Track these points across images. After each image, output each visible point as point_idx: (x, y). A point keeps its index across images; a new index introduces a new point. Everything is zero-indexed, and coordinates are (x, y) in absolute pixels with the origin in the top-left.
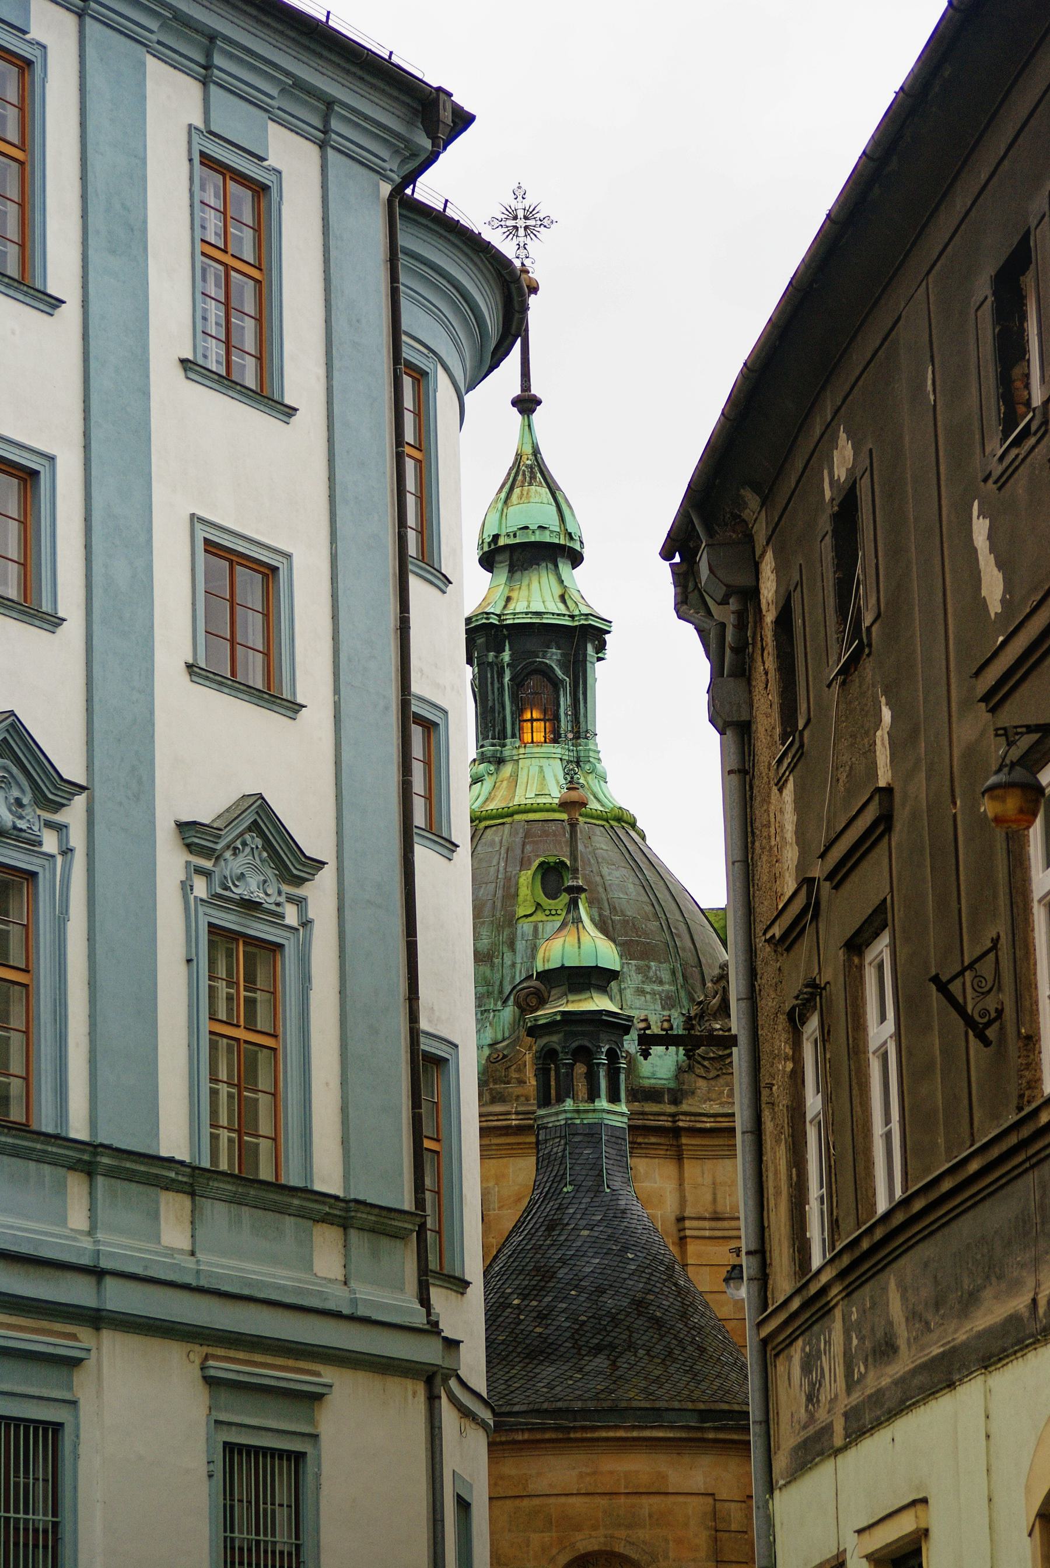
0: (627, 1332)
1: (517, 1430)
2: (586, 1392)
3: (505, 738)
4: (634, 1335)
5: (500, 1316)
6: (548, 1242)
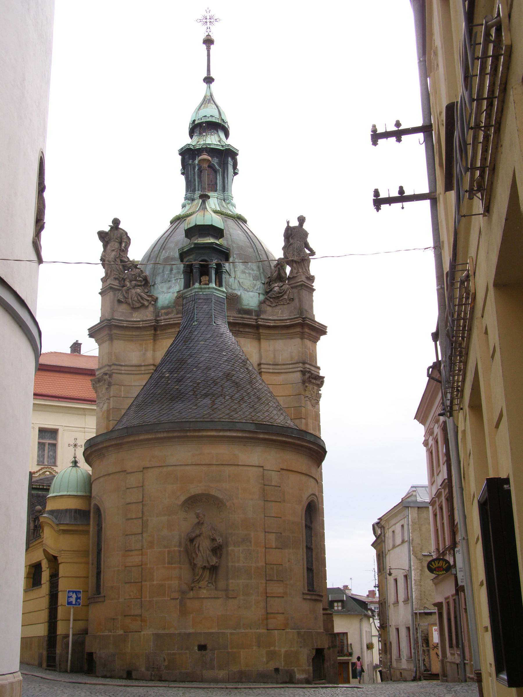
0: (221, 388)
1: (161, 432)
2: (198, 415)
3: (195, 191)
4: (224, 389)
5: (159, 382)
6: (184, 348)
